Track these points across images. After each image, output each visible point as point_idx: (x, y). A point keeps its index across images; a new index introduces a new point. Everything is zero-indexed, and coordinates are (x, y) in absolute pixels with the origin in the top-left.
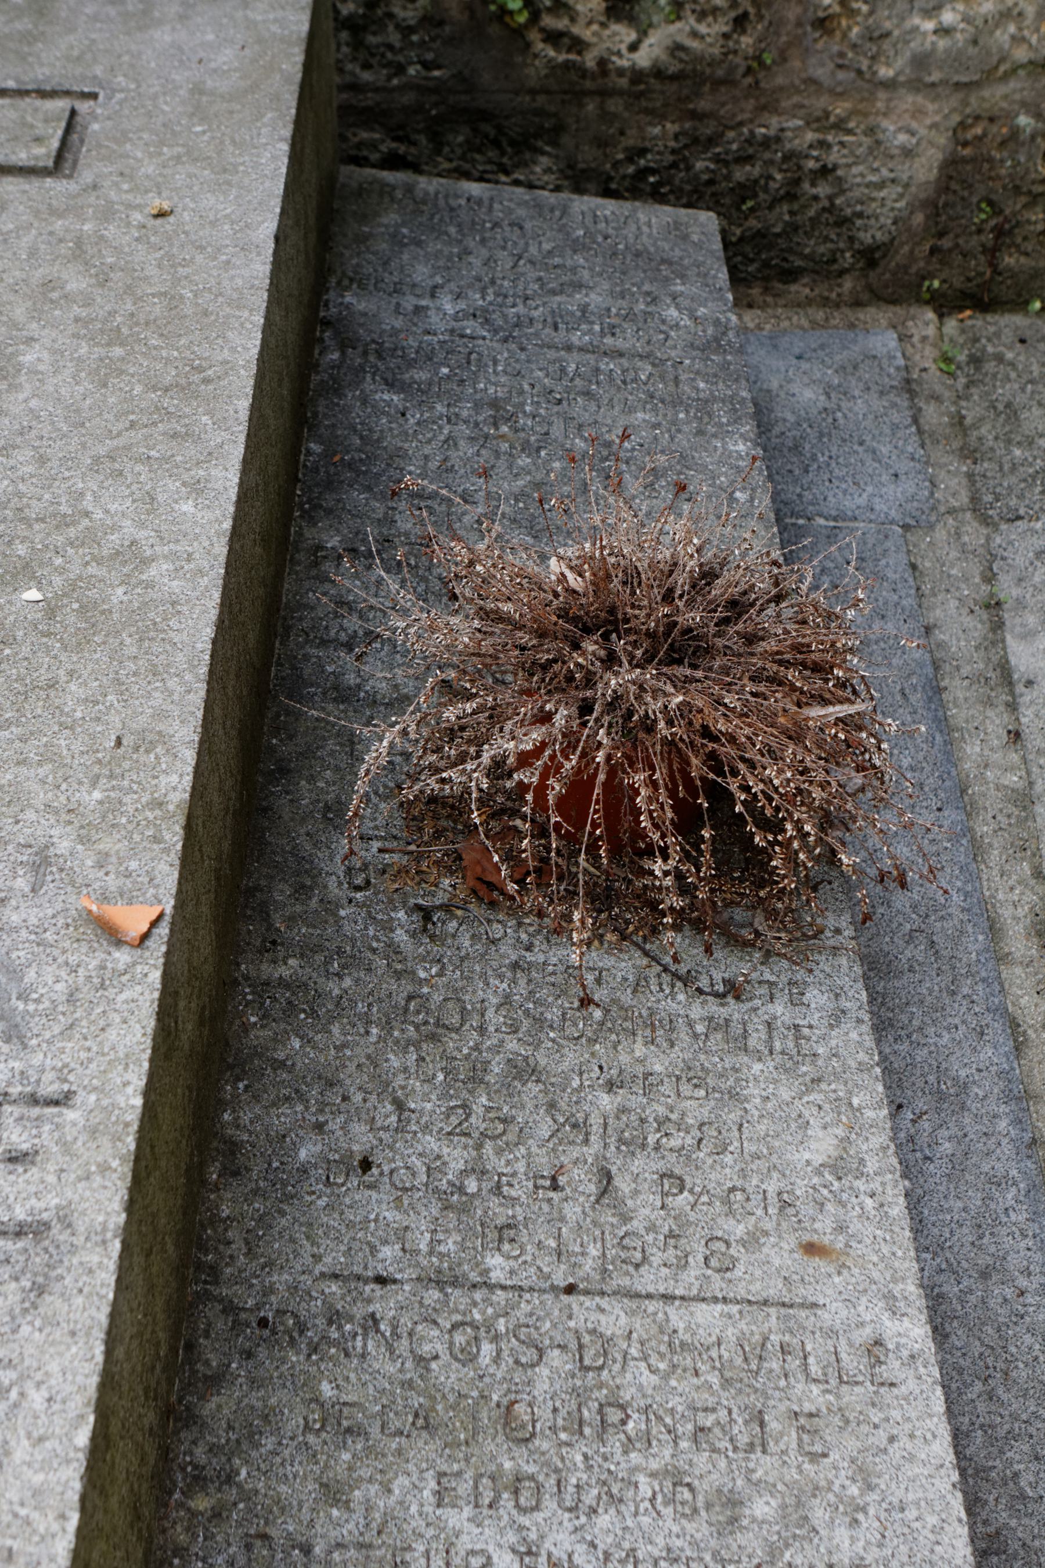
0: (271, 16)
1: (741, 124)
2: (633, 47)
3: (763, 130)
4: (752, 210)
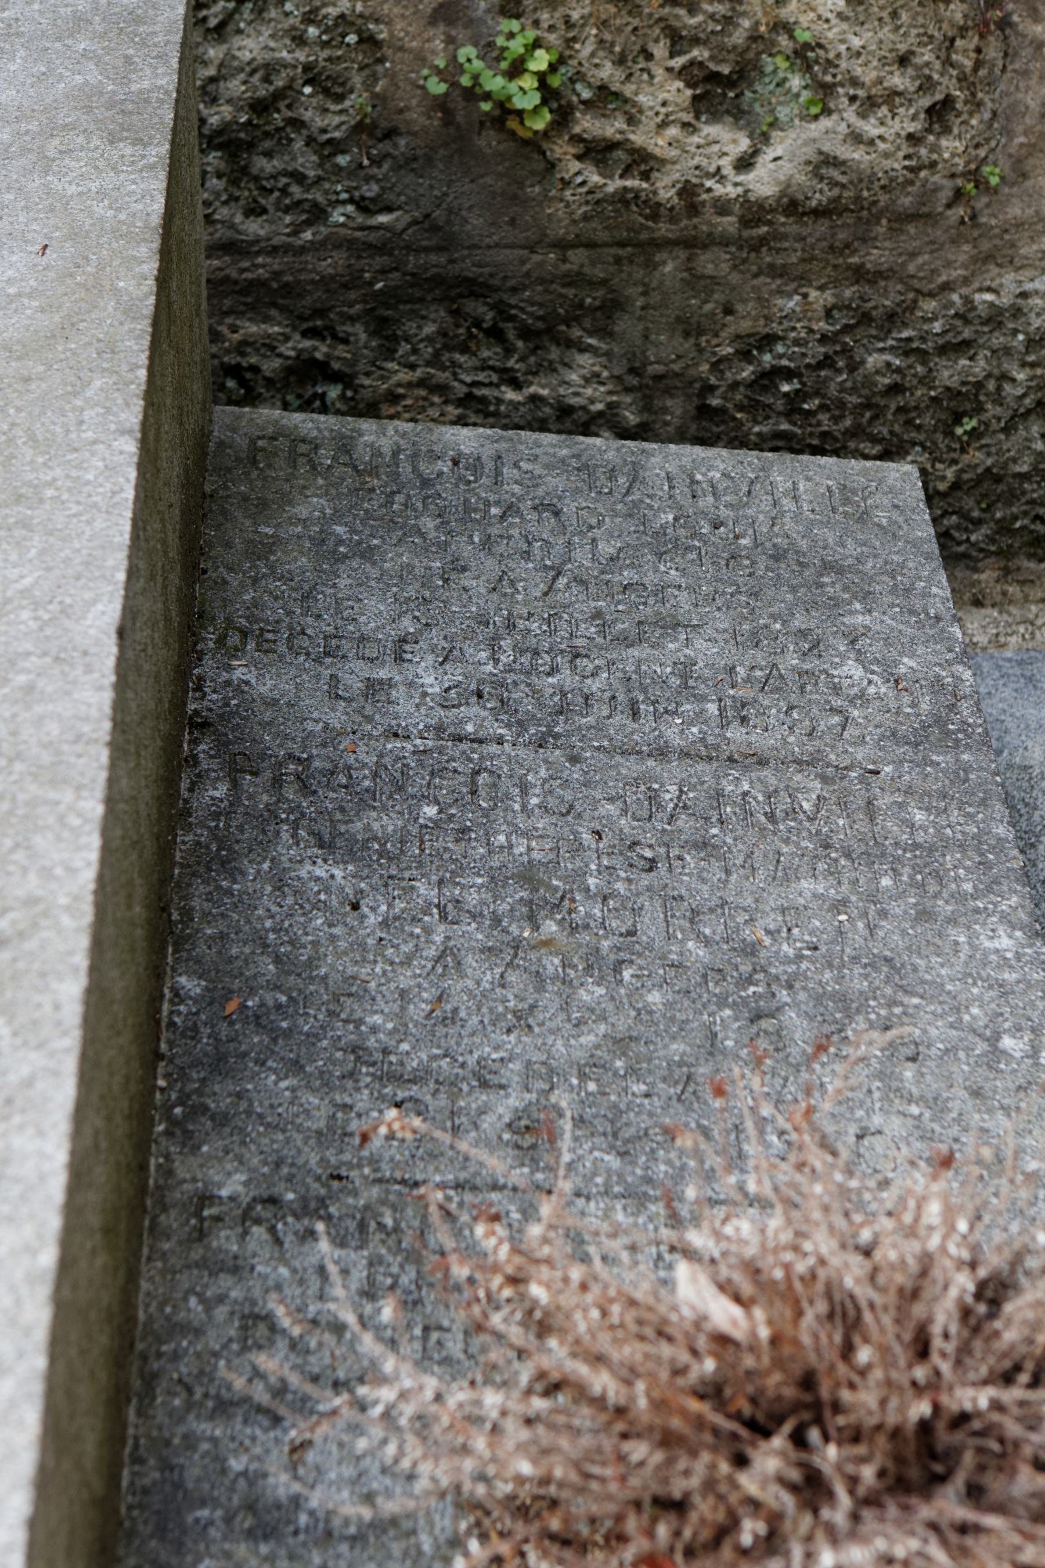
0: (94, 186)
1: (947, 287)
2: (745, 163)
3: (989, 297)
4: (973, 433)
